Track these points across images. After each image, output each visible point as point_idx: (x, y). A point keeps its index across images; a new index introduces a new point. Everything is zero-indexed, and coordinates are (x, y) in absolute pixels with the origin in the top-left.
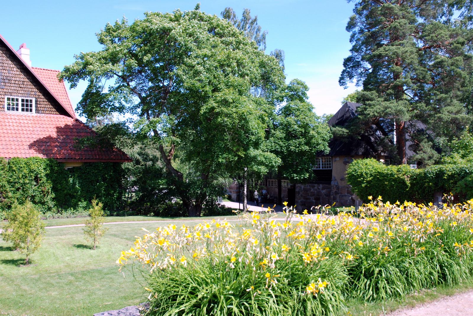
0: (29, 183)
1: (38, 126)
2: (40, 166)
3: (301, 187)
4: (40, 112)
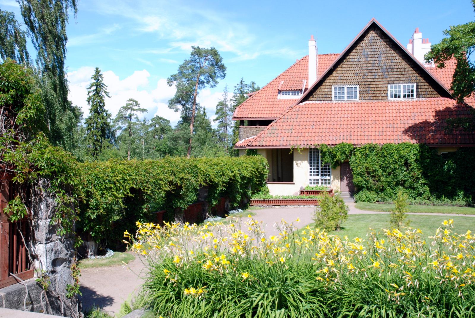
0: (399, 168)
1: (416, 111)
2: (410, 152)
4: (421, 96)
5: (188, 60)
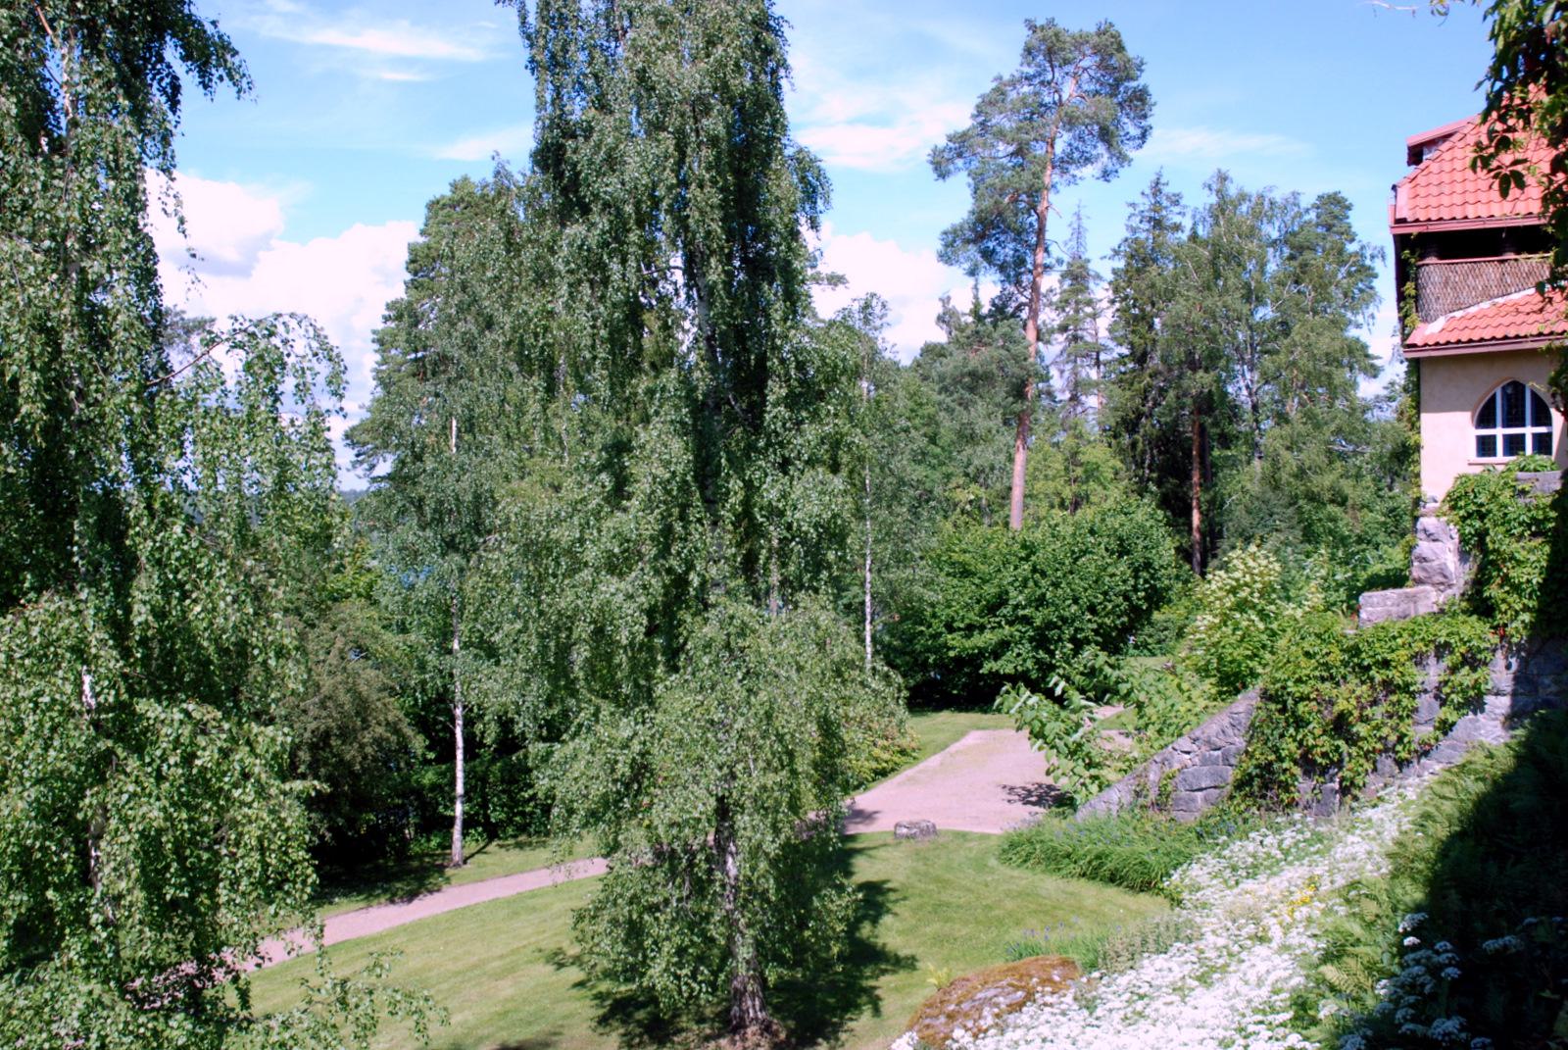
5: (1006, 77)
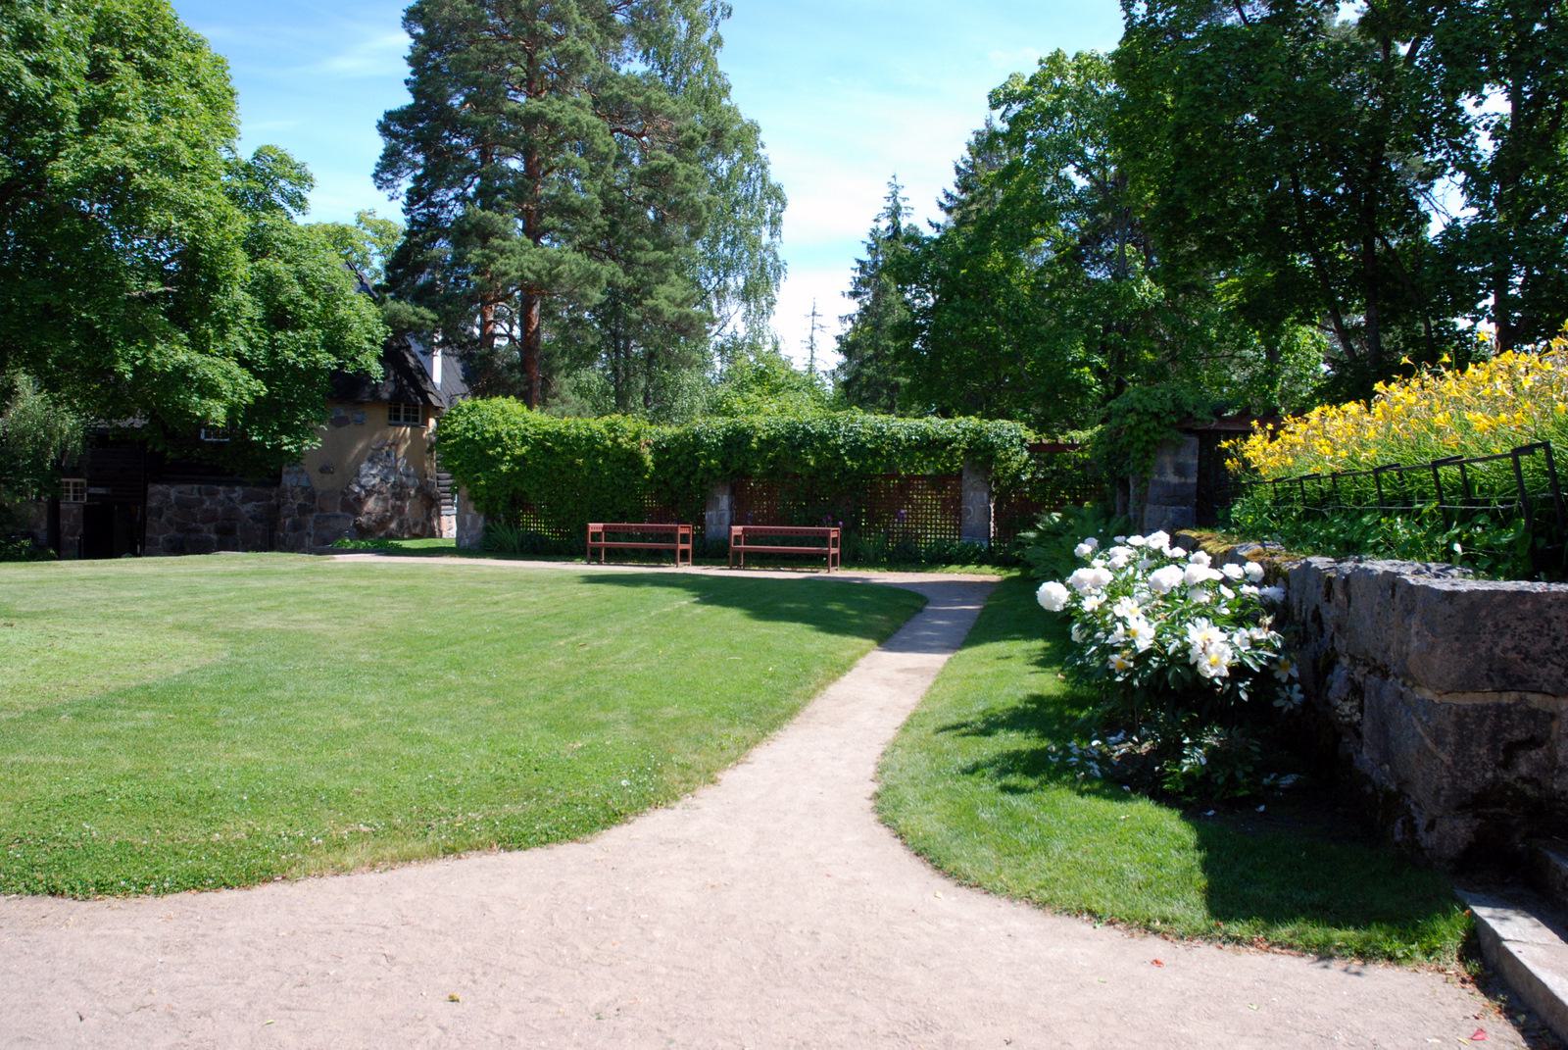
3: (168, 496)
